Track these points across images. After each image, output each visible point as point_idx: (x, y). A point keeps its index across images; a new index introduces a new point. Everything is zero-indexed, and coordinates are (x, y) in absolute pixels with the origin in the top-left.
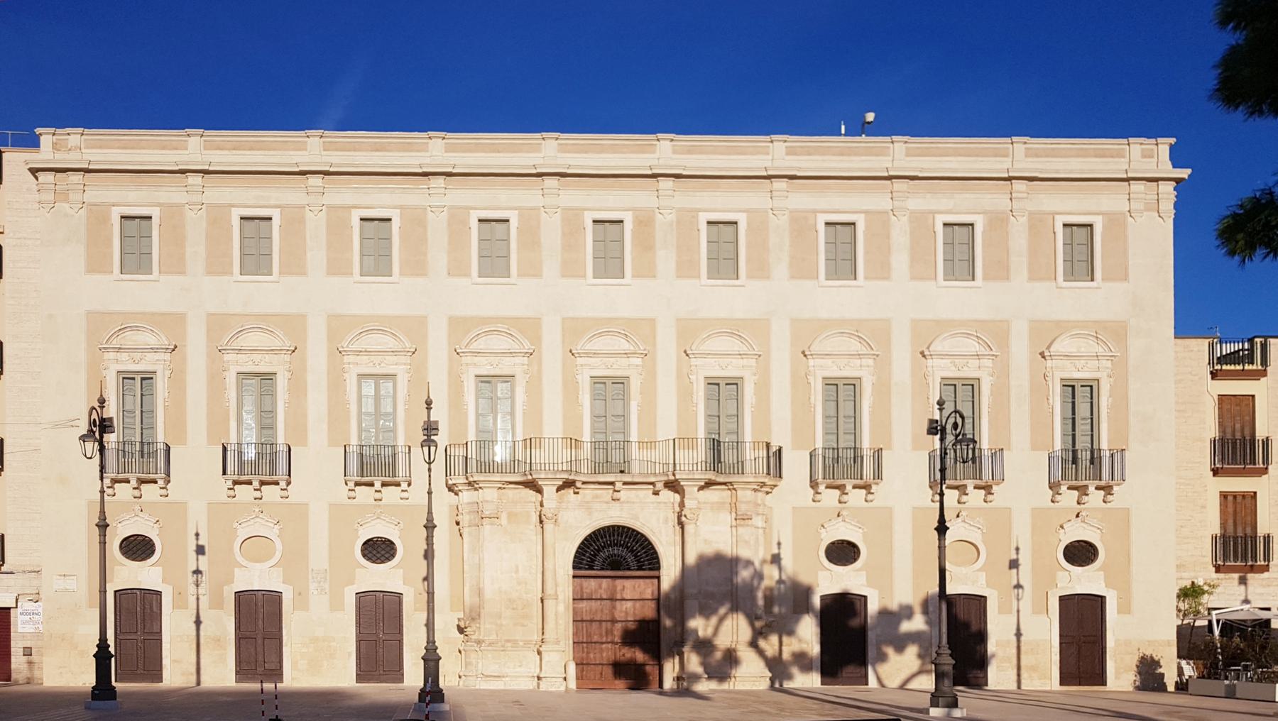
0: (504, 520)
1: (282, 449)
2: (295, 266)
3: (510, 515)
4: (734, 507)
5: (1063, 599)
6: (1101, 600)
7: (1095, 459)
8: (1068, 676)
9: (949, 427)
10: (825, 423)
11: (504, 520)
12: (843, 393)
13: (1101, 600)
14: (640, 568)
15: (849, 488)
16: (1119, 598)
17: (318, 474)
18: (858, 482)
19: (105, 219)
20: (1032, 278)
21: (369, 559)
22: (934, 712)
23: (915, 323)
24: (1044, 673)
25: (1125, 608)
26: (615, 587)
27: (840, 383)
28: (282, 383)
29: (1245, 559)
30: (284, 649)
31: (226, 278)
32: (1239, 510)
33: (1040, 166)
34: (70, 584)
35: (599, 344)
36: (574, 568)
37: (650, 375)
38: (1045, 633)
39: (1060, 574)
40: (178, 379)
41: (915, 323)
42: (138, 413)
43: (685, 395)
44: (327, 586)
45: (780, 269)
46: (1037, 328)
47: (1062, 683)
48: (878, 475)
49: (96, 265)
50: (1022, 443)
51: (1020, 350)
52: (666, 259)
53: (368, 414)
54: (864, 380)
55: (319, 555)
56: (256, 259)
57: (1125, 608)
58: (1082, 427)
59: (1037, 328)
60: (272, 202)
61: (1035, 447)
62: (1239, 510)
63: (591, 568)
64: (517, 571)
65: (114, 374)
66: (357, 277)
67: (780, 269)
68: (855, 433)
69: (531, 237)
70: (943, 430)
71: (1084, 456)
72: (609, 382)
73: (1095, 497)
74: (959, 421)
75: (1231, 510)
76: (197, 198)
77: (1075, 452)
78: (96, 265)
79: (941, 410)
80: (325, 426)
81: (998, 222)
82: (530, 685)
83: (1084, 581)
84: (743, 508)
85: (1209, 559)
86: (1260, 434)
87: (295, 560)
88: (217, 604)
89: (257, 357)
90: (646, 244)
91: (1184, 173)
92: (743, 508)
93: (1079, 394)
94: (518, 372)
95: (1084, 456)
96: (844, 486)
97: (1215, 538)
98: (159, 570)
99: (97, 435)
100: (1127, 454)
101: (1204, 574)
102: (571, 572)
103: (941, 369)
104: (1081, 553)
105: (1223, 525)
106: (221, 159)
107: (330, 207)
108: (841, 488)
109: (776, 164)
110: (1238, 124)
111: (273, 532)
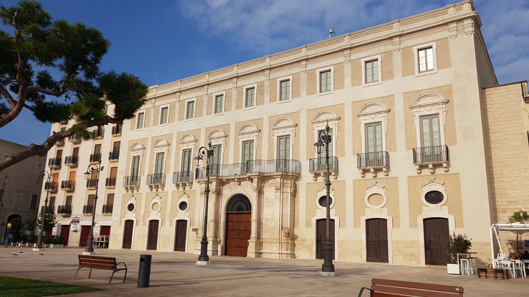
1: (444, 149)
6: (445, 221)
8: (124, 247)
13: (445, 221)
17: (402, 165)
19: (158, 110)
22: (199, 263)
23: (207, 129)
31: (314, 96)
35: (423, 102)
39: (424, 208)
40: (391, 123)
41: (207, 129)
46: (407, 95)
52: (267, 97)
53: (282, 150)
58: (159, 167)
59: (407, 95)
61: (407, 149)
63: (232, 210)
65: (364, 125)
66: (244, 108)
67: (304, 93)
76: (398, 46)
81: (261, 85)
87: (393, 205)
90: (261, 93)
94: (440, 111)
98: (446, 207)
104: (434, 197)
111: (382, 192)
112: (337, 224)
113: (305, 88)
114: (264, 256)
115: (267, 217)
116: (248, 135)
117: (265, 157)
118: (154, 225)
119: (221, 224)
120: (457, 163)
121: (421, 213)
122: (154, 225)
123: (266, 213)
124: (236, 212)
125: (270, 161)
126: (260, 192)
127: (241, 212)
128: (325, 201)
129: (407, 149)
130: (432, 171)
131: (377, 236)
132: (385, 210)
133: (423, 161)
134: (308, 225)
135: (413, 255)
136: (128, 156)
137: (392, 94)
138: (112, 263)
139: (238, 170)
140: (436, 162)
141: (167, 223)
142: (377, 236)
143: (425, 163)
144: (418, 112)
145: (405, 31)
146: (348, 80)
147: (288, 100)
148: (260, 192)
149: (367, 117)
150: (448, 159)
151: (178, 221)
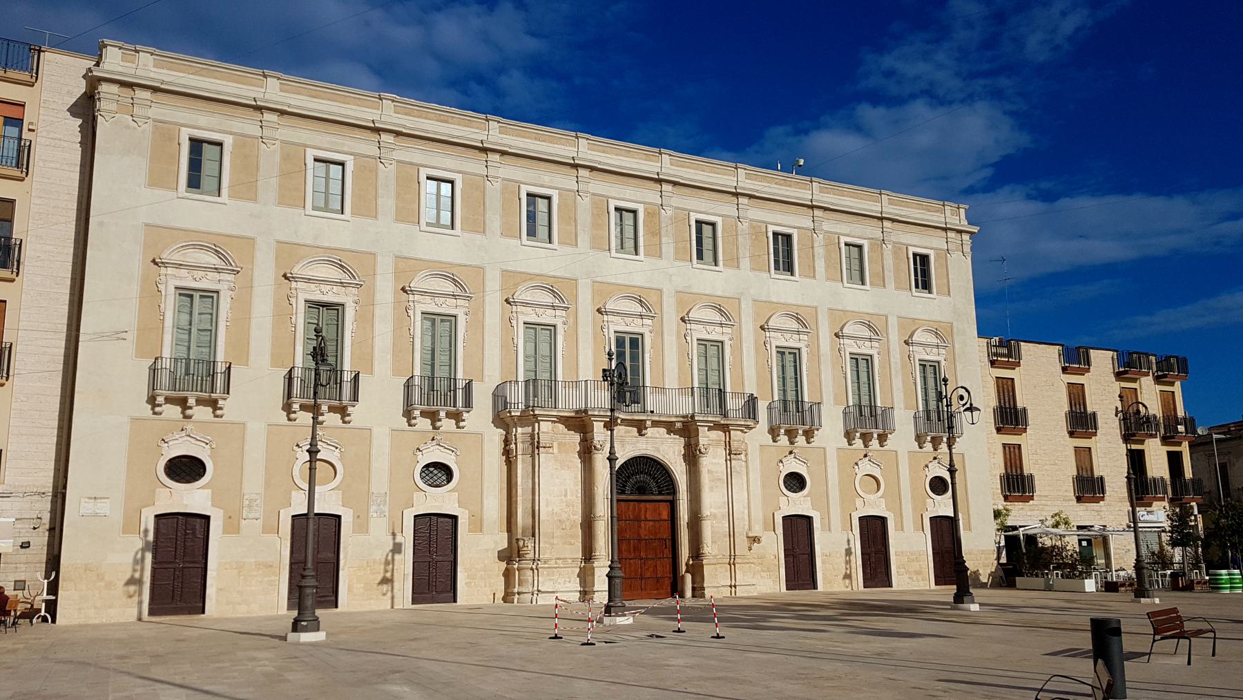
0: (555, 450)
3: (559, 444)
4: (728, 444)
5: (784, 518)
6: (883, 520)
7: (873, 414)
10: (525, 361)
11: (555, 450)
12: (790, 359)
14: (660, 493)
15: (191, 401)
18: (336, 403)
20: (897, 288)
21: (172, 479)
24: (764, 579)
26: (640, 509)
27: (787, 351)
29: (1024, 492)
30: (341, 573)
32: (1013, 455)
33: (701, 178)
34: (103, 507)
37: (659, 333)
42: (194, 330)
43: (685, 355)
44: (386, 509)
45: (584, 239)
47: (937, 584)
48: (355, 398)
50: (381, 363)
51: (895, 338)
54: (347, 305)
55: (380, 482)
57: (232, 526)
60: (346, 149)
62: (1013, 455)
64: (566, 495)
67: (584, 239)
68: (212, 345)
69: (248, 166)
71: (866, 411)
72: (197, 295)
73: (447, 424)
74: (966, 395)
77: (860, 406)
78: (157, 180)
80: (389, 357)
82: (726, 592)
83: (798, 504)
87: (895, 499)
89: (325, 288)
90: (655, 232)
91: (975, 229)
92: (734, 445)
93: (930, 369)
95: (866, 411)
96: (185, 400)
101: (1001, 504)
103: (617, 325)
104: (186, 469)
106: (890, 210)
107: (398, 161)
108: (183, 403)
109: (139, 72)
110: (1012, 206)
112: (817, 524)
113: (274, 182)
114: (708, 593)
115: (713, 510)
117: (671, 381)
118: (874, 533)
119: (603, 529)
122: (874, 533)
123: (712, 501)
124: (632, 497)
126: (692, 456)
127: (645, 498)
131: (315, 555)
135: (918, 573)
136: (678, 332)
141: (251, 525)
142: (315, 555)
144: (173, 280)
148: (692, 456)
149: (183, 272)
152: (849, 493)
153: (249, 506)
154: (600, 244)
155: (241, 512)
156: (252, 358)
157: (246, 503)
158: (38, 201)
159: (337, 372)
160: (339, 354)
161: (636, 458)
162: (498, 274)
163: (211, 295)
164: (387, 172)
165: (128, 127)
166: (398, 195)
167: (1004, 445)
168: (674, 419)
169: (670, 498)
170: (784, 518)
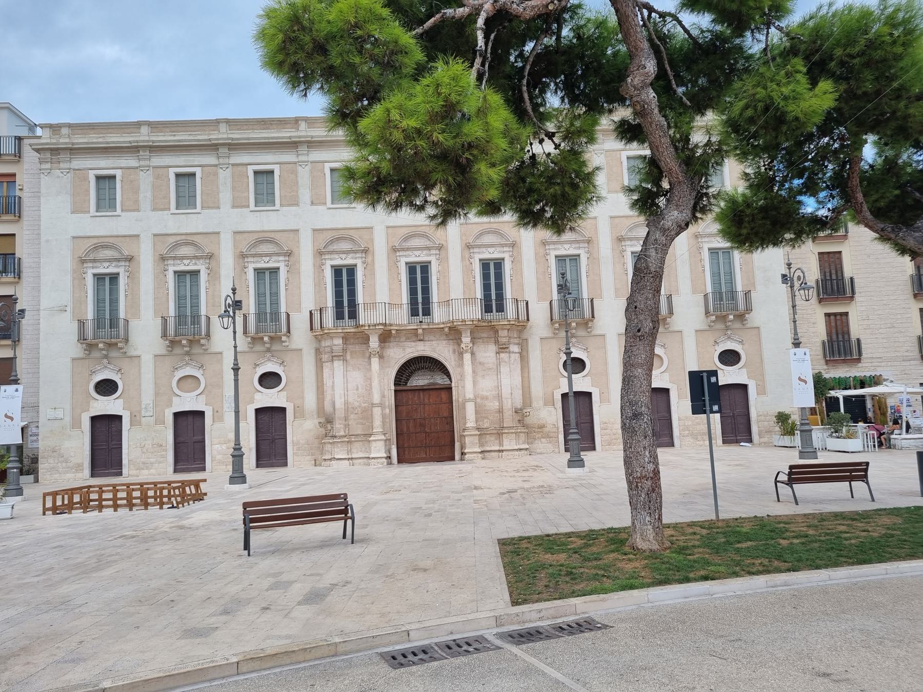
1: (283, 317)
2: (212, 204)
5: (258, 411)
9: (795, 279)
16: (757, 385)
19: (86, 179)
25: (762, 391)
28: (203, 277)
32: (838, 326)
36: (395, 384)
38: (80, 445)
39: (175, 399)
49: (78, 209)
56: (186, 199)
57: (762, 391)
60: (196, 163)
62: (838, 326)
64: (357, 389)
70: (792, 280)
75: (833, 324)
78: (78, 209)
79: (789, 269)
84: (504, 340)
85: (821, 356)
86: (847, 273)
88: (550, 402)
97: (824, 342)
99: (231, 314)
100: (753, 294)
101: (822, 367)
102: (393, 388)
105: (829, 334)
107: (233, 165)
111: (198, 373)
112: (595, 398)
116: (418, 253)
120: (756, 317)
121: (170, 404)
125: (468, 301)
128: (576, 365)
129: (156, 316)
130: (187, 349)
132: (666, 376)
133: (258, 330)
134: (550, 402)
137: (135, 233)
138: (340, 504)
139: (475, 312)
140: (191, 338)
143: (177, 338)
145: (78, 144)
146: (226, 196)
147: (115, 213)
150: (289, 331)
151: (179, 416)
152: (162, 394)
153: (146, 408)
154: (238, 204)
155: (140, 412)
156: (142, 312)
157: (143, 406)
158: (28, 232)
159: (577, 301)
160: (579, 289)
161: (431, 358)
162: (310, 233)
163: (275, 271)
164: (304, 173)
165: (59, 177)
166: (234, 189)
167: (828, 315)
168: (442, 326)
169: (705, 375)
170: (258, 411)
